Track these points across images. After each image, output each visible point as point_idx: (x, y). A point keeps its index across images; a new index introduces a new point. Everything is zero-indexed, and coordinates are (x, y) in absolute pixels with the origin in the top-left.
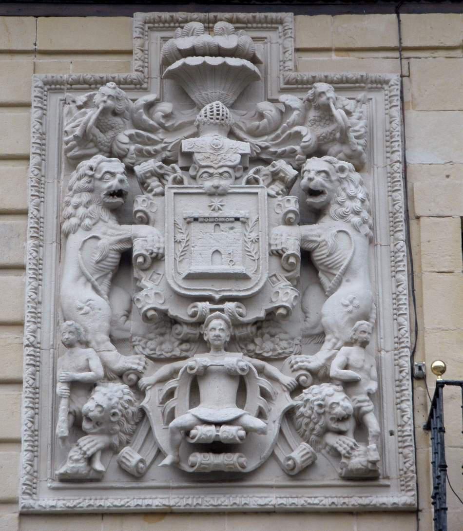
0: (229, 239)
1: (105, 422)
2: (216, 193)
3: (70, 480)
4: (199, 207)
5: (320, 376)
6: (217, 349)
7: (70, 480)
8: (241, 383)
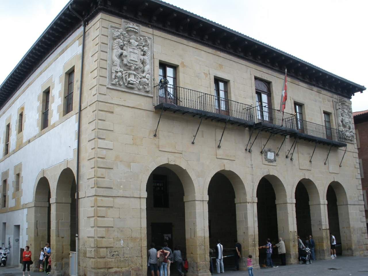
0: (135, 56)
1: (118, 78)
2: (134, 49)
3: (113, 84)
4: (132, 50)
5: (144, 77)
6: (132, 70)
7: (113, 84)
8: (135, 75)
